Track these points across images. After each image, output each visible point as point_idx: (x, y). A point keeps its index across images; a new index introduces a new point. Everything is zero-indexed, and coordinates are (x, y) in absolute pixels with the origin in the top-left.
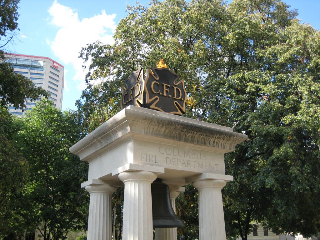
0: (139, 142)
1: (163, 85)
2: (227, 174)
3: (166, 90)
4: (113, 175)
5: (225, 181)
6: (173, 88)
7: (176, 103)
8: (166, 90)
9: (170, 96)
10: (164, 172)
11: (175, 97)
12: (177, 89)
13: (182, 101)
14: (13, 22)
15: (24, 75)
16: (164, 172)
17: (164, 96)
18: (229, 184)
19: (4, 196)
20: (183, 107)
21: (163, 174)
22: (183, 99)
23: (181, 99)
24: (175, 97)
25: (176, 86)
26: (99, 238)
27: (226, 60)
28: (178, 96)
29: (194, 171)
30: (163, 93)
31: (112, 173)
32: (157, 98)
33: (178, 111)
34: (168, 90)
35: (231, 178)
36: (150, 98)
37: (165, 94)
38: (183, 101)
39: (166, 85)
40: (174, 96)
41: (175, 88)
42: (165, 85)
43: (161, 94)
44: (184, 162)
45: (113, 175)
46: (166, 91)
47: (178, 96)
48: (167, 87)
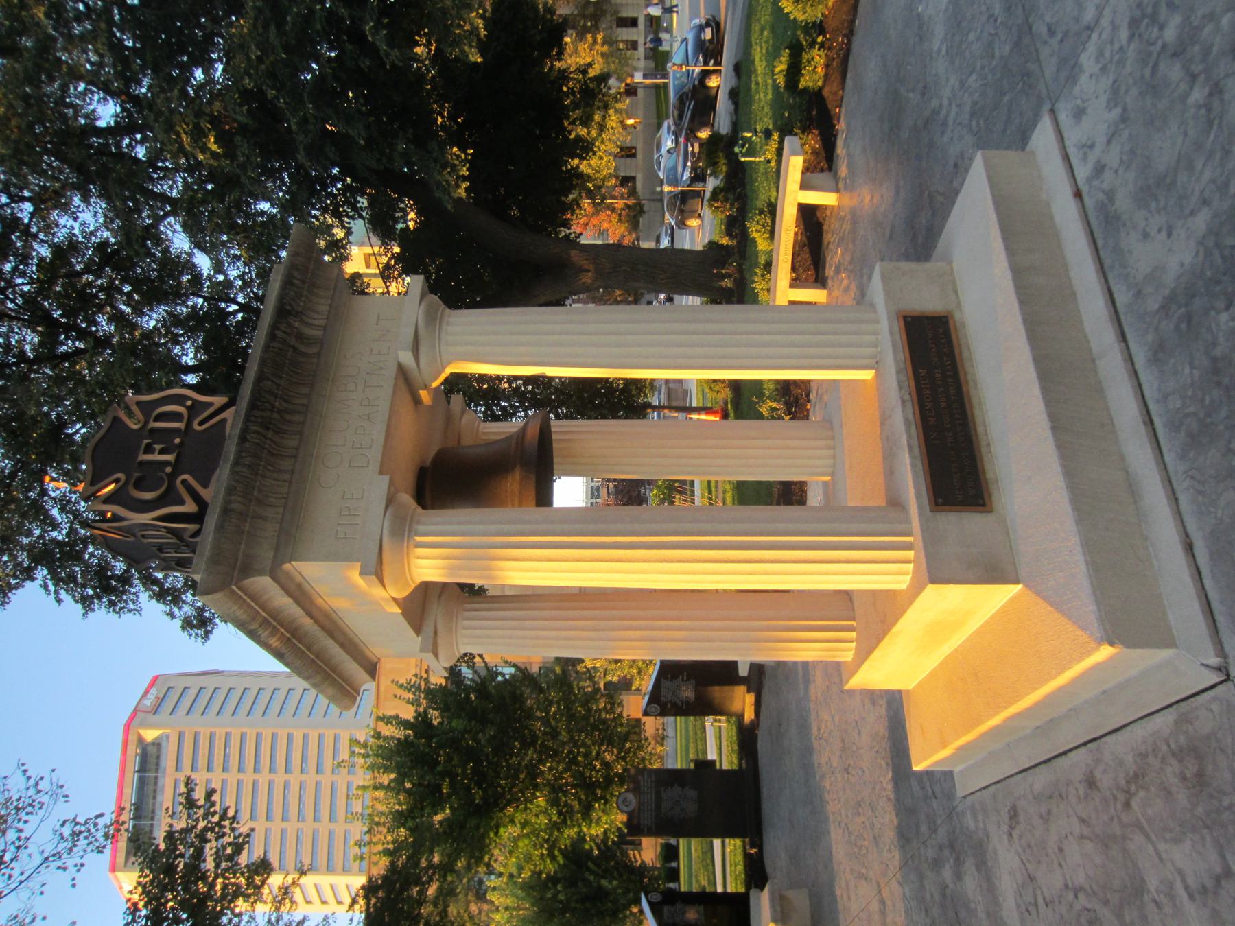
0: (289, 542)
1: (142, 463)
5: (422, 297)
7: (200, 424)
9: (177, 441)
12: (157, 419)
13: (193, 404)
14: (908, 588)
15: (805, 648)
19: (6, 119)
20: (211, 404)
23: (188, 408)
25: (146, 423)
26: (556, 432)
27: (78, 268)
30: (167, 463)
33: (224, 421)
34: (158, 447)
36: (182, 502)
38: (195, 401)
40: (177, 431)
43: (169, 469)
46: (162, 452)
47: (176, 416)
48: (149, 449)
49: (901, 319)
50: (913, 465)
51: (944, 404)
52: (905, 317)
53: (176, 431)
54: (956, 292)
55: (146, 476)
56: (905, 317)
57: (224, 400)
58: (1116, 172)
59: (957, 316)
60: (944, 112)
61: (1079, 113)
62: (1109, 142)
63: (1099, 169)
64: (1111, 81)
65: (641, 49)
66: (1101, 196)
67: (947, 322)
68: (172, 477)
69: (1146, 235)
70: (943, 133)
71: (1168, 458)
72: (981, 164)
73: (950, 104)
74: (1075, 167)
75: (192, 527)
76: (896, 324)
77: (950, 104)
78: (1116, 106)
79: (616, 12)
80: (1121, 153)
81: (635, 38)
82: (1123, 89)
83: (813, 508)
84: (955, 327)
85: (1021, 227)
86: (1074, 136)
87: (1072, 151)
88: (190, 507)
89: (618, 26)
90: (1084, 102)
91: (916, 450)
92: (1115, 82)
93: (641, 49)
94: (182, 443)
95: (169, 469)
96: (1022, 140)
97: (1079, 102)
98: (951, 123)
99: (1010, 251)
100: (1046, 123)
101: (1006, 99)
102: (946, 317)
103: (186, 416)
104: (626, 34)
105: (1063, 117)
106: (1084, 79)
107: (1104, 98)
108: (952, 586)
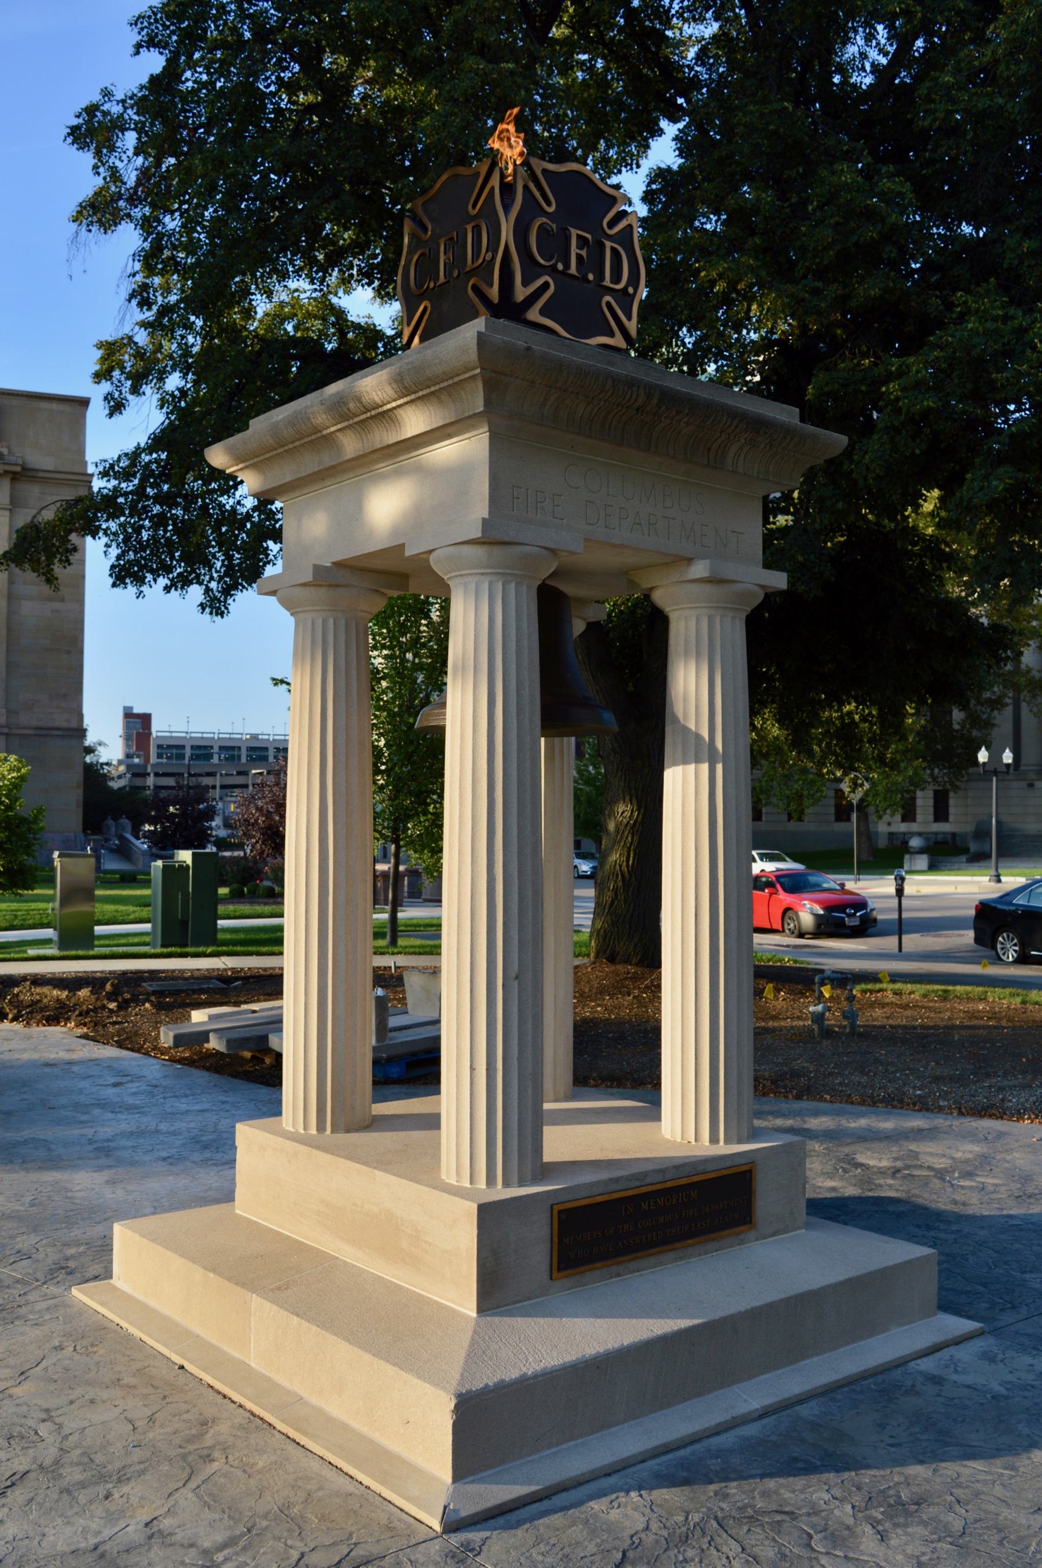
2: (767, 565)
3: (579, 251)
4: (408, 553)
6: (602, 246)
7: (549, 204)
8: (579, 251)
9: (591, 277)
10: (239, 1126)
11: (607, 282)
16: (239, 1126)
17: (572, 276)
18: (770, 597)
20: (629, 318)
21: (238, 1121)
22: (631, 290)
24: (607, 282)
25: (610, 238)
28: (617, 277)
29: (690, 1154)
30: (567, 266)
31: (403, 545)
32: (546, 286)
34: (584, 253)
35: (779, 580)
36: (525, 284)
37: (573, 270)
39: (578, 236)
41: (608, 244)
42: (574, 232)
43: (560, 266)
44: (637, 520)
45: (408, 553)
46: (579, 257)
47: (617, 277)
48: (582, 242)
49: (747, 1168)
50: (598, 1183)
51: (661, 1220)
52: (750, 1171)
53: (601, 276)
54: (774, 1234)
55: (555, 244)
56: (750, 1171)
57: (633, 333)
58: (938, 1395)
59: (752, 1234)
60: (942, 1226)
61: (989, 1357)
62: (969, 1387)
63: (937, 1380)
64: (1033, 1383)
65: (903, 827)
66: (909, 1383)
67: (744, 1223)
68: (553, 270)
69: (882, 1426)
70: (918, 1226)
71: (652, 1464)
72: (924, 1254)
73: (953, 1232)
74: (931, 1358)
75: (494, 293)
76: (743, 1161)
77: (953, 1232)
78: (1007, 1389)
79: (956, 789)
80: (960, 1398)
81: (919, 818)
82: (1026, 1393)
83: (370, 1107)
84: (739, 1234)
85: (860, 1303)
86: (965, 1353)
87: (945, 1354)
88: (521, 293)
89: (936, 792)
90: (1002, 1361)
91: (613, 1187)
92: (1033, 1386)
93: (903, 827)
94: (589, 281)
95: (560, 266)
96: (946, 1306)
97: (1000, 1357)
98: (932, 1233)
99: (836, 1288)
100: (968, 1325)
101: (981, 1289)
102: (750, 1222)
103: (617, 287)
104: (924, 801)
105: (979, 1344)
106: (1028, 1360)
107: (1010, 1377)
108: (475, 1232)
